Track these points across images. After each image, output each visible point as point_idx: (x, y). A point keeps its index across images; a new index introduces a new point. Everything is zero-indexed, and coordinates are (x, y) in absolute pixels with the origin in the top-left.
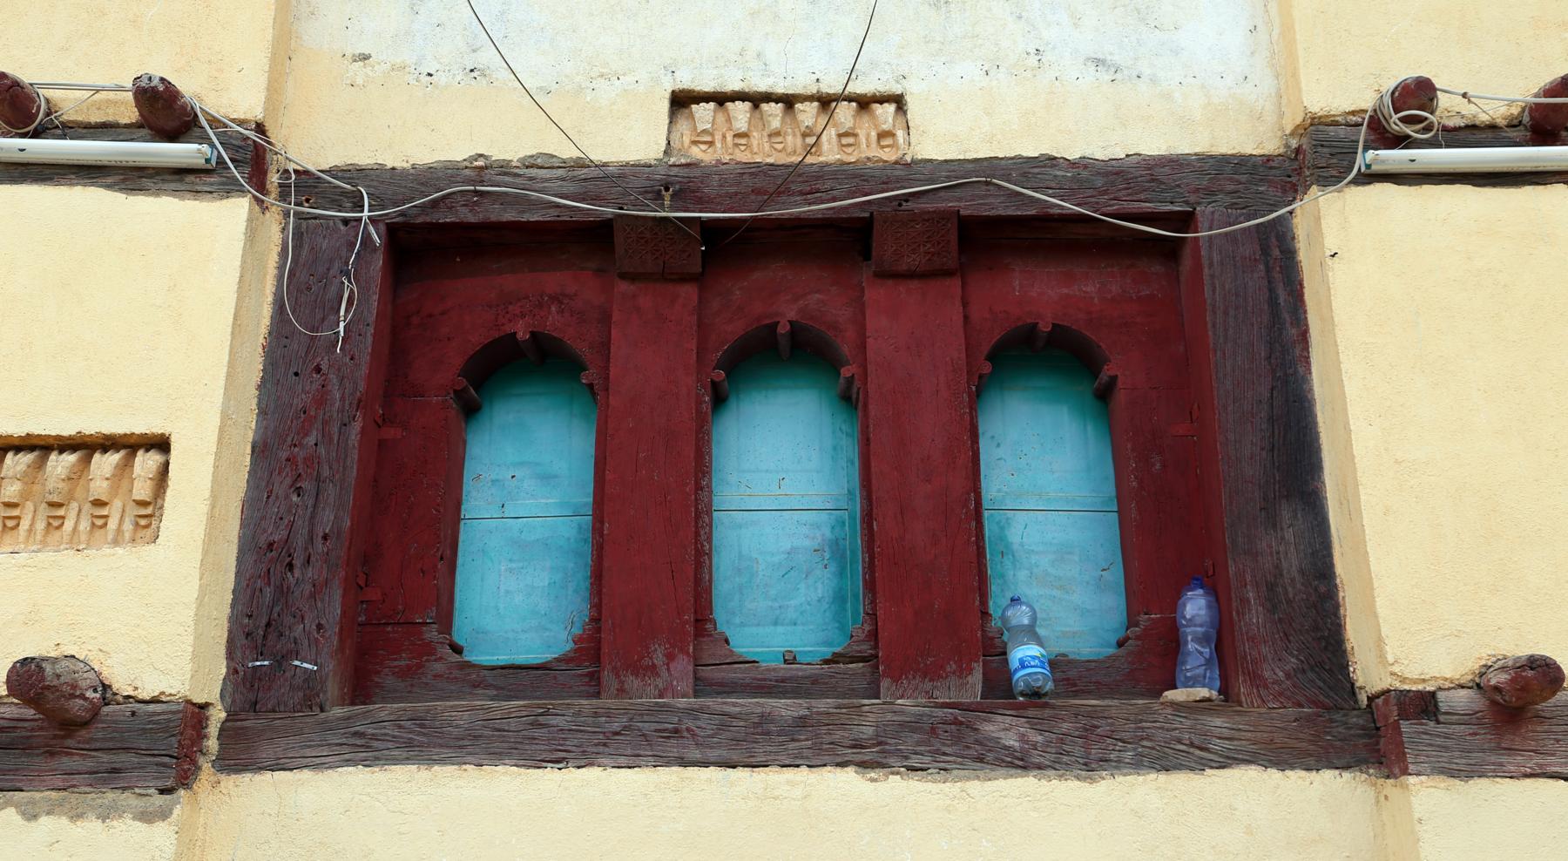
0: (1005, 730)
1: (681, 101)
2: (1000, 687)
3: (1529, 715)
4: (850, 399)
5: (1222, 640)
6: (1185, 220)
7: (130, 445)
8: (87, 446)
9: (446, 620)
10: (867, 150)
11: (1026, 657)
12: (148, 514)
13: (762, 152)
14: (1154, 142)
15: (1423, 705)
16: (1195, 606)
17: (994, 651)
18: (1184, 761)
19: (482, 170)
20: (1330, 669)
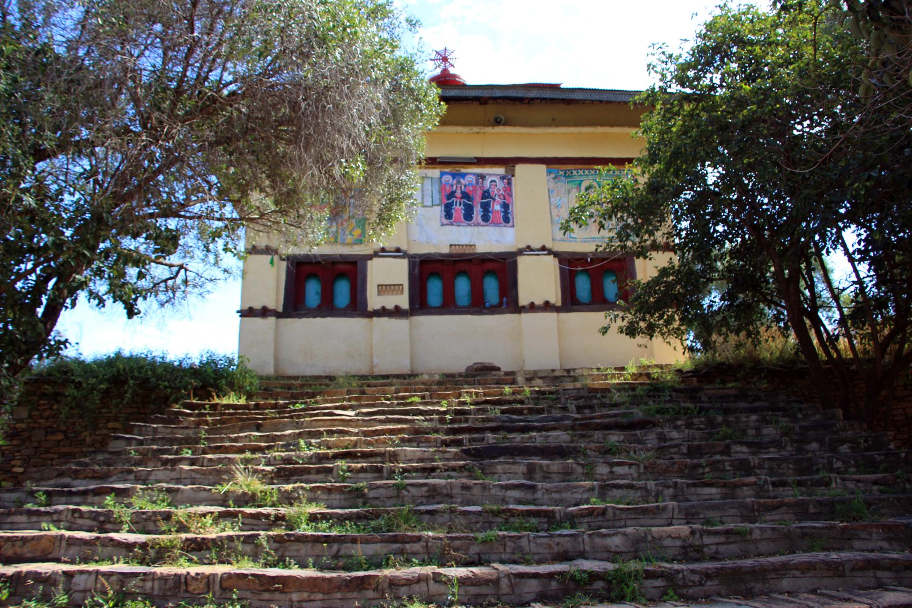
0: (485, 311)
1: (451, 245)
2: (485, 307)
3: (646, 388)
4: (469, 278)
5: (507, 304)
6: (505, 259)
7: (399, 285)
8: (395, 285)
9: (304, 301)
10: (471, 251)
11: (487, 304)
12: (402, 292)
13: (460, 252)
14: (502, 250)
15: (523, 307)
16: (505, 299)
17: (484, 304)
18: (317, 415)
19: (429, 254)
20: (144, 454)
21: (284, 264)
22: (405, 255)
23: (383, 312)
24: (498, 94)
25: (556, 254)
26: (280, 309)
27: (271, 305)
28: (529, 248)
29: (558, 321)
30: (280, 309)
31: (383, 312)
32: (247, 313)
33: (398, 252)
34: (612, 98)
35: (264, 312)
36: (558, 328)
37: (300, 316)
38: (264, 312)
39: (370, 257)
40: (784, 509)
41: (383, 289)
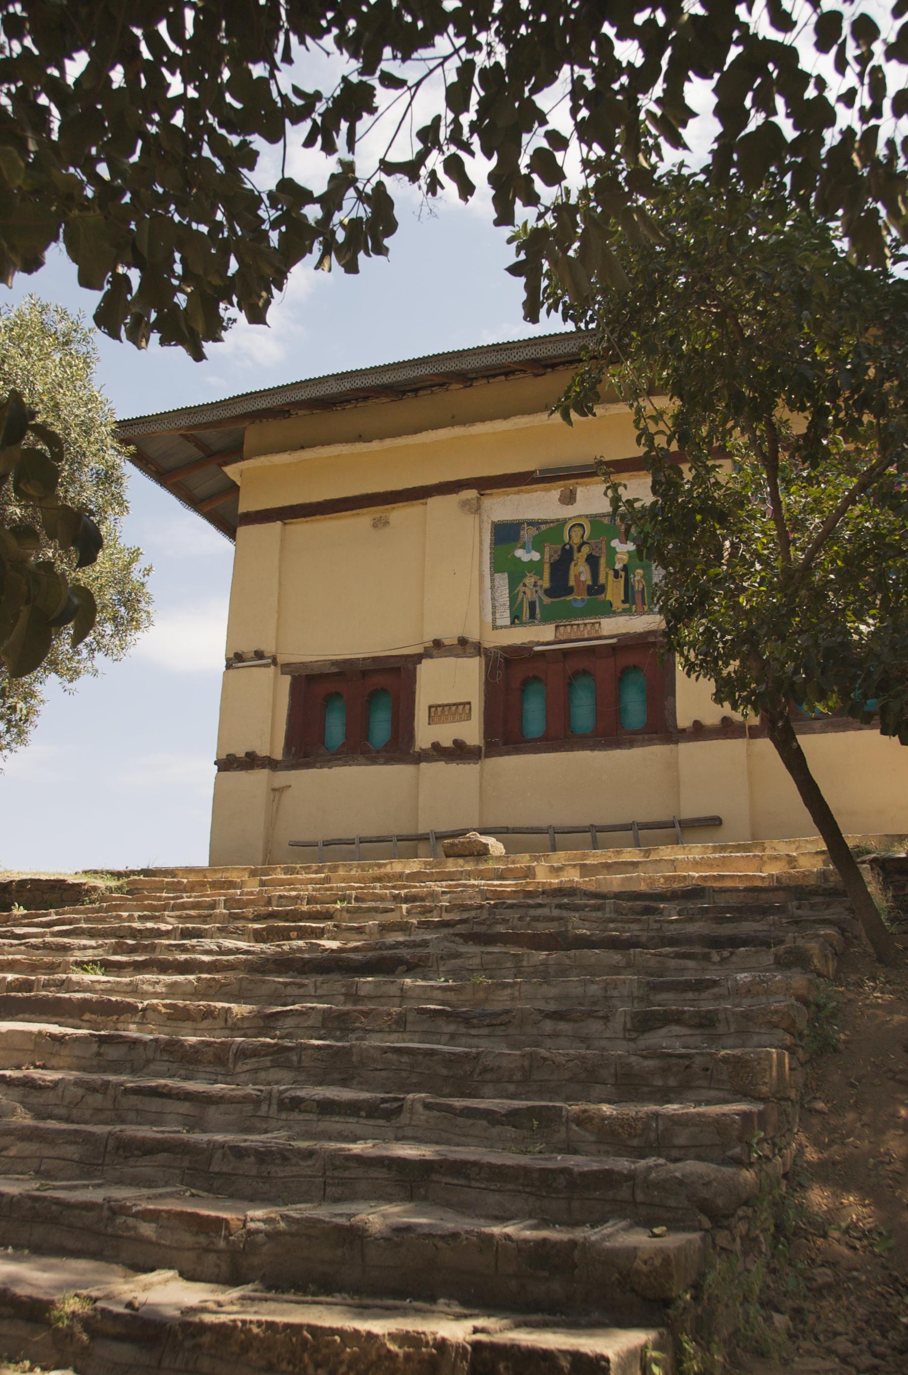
7: (464, 704)
12: (469, 717)
21: (288, 679)
22: (478, 649)
23: (438, 753)
24: (263, 404)
25: (286, 668)
26: (278, 755)
27: (263, 751)
28: (437, 643)
29: (749, 756)
30: (278, 755)
31: (438, 753)
32: (226, 764)
33: (464, 646)
34: (466, 365)
35: (250, 762)
36: (481, 787)
37: (518, 751)
38: (250, 762)
39: (418, 658)
40: (162, 1157)
41: (438, 712)
